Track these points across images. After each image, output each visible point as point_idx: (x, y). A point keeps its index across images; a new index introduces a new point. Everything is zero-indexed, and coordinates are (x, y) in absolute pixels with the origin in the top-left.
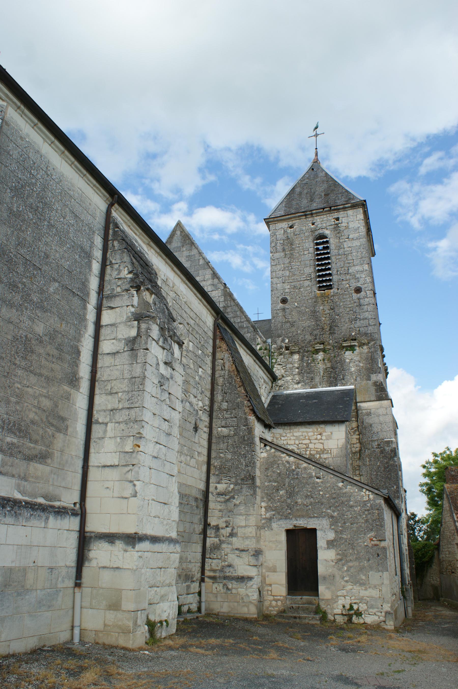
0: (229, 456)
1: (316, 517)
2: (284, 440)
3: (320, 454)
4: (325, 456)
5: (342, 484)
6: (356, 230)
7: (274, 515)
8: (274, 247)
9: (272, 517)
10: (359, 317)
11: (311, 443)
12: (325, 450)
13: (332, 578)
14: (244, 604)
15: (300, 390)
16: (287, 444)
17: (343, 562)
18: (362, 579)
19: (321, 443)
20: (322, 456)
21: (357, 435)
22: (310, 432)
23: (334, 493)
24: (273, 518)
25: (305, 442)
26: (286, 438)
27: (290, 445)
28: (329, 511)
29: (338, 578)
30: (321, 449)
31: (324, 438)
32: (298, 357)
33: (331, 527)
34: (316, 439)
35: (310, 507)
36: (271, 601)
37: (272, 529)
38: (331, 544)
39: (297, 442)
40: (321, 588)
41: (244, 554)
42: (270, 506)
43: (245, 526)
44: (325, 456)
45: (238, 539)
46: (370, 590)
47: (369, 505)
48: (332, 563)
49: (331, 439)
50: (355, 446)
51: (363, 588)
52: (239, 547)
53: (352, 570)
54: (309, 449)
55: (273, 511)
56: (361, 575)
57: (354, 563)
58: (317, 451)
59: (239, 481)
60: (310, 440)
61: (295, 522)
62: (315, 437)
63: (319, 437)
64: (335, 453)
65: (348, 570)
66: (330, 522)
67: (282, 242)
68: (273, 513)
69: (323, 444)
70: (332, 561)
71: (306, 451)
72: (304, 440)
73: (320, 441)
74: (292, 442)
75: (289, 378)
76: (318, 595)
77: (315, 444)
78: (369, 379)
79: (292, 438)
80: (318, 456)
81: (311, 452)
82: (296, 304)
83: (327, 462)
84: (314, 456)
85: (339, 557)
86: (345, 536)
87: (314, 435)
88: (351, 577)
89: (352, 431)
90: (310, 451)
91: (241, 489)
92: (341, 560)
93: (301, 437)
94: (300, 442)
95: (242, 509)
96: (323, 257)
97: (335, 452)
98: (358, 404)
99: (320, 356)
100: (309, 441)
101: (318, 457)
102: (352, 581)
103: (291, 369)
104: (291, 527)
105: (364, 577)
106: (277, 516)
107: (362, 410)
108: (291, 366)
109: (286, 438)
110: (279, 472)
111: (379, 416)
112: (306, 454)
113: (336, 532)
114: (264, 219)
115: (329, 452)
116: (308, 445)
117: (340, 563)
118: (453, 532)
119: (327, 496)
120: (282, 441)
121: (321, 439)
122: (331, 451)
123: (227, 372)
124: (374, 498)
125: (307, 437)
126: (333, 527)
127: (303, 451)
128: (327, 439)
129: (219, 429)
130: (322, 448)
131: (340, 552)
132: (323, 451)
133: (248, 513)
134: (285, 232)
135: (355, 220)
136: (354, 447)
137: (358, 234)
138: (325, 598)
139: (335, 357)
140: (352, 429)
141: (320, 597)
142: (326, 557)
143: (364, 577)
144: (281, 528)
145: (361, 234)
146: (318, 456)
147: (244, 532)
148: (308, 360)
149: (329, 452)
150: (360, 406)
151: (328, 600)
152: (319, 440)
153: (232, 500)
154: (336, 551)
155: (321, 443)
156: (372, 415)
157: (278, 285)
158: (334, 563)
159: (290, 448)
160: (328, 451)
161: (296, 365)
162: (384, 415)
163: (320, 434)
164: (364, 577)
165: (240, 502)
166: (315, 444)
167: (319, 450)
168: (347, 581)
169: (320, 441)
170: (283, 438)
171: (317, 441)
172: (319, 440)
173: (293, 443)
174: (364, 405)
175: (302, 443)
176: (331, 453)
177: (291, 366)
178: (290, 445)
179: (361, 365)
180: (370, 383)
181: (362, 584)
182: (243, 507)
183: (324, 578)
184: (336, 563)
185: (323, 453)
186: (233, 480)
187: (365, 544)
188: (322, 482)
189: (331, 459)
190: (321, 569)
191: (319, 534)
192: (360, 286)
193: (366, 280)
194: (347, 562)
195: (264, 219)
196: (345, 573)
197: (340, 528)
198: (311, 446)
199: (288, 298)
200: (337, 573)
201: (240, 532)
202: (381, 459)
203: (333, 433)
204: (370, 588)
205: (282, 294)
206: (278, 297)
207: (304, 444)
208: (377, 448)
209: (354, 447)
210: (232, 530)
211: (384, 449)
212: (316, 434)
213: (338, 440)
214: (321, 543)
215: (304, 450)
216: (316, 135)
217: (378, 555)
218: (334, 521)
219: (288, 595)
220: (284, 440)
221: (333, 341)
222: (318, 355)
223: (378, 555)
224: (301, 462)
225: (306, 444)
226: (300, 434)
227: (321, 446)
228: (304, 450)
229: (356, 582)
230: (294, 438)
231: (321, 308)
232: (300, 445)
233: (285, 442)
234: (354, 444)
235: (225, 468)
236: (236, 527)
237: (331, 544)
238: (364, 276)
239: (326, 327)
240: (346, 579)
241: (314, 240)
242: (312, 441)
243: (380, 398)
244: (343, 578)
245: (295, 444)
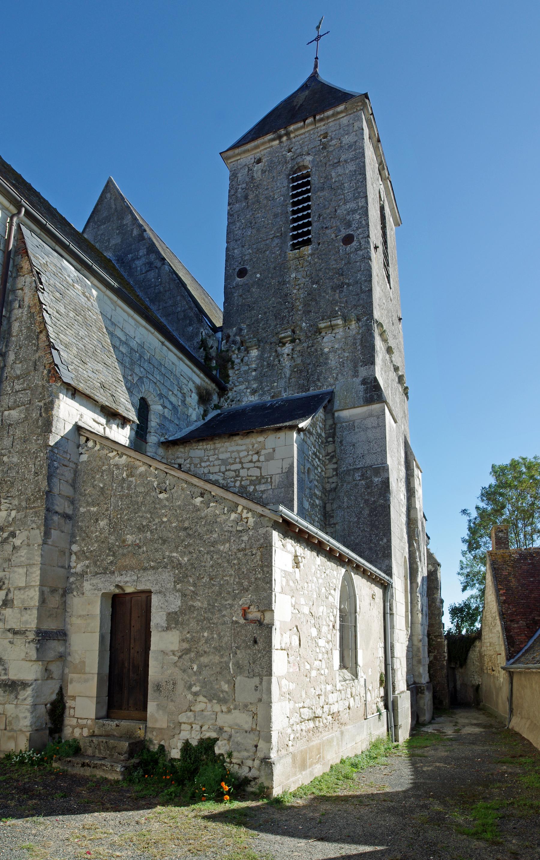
0: (15, 460)
1: (153, 568)
2: (204, 467)
3: (255, 485)
4: (262, 487)
5: (201, 499)
6: (350, 147)
7: (87, 567)
8: (233, 195)
9: (85, 570)
10: (347, 281)
11: (243, 468)
12: (263, 477)
13: (171, 687)
14: (10, 734)
15: (254, 399)
16: (209, 473)
17: (193, 655)
18: (222, 691)
19: (257, 467)
20: (257, 487)
21: (334, 463)
22: (243, 451)
23: (187, 519)
24: (87, 573)
25: (233, 467)
26: (208, 463)
27: (212, 474)
28: (175, 554)
29: (180, 686)
30: (257, 477)
31: (262, 458)
32: (256, 354)
33: (175, 586)
34: (251, 461)
35: (145, 549)
36: (74, 728)
37: (83, 594)
38: (174, 620)
39: (223, 469)
40: (151, 707)
41: (19, 640)
42: (83, 551)
43: (25, 588)
44: (262, 487)
45: (13, 611)
46: (236, 713)
47: (245, 538)
48: (173, 657)
49: (273, 459)
50: (331, 480)
51: (224, 709)
52: (14, 626)
53: (206, 673)
54: (239, 478)
55: (87, 558)
56: (223, 683)
57: (211, 657)
58: (251, 481)
59: (24, 504)
60: (241, 463)
61: (118, 579)
62: (249, 458)
63: (255, 458)
64: (277, 481)
65: (199, 672)
66: (175, 576)
67: (244, 186)
68: (87, 562)
69: (260, 468)
70: (174, 654)
71: (235, 481)
72: (233, 464)
73: (257, 464)
74: (216, 469)
75: (242, 387)
76: (144, 719)
77: (248, 469)
78: (356, 374)
79: (216, 463)
80: (251, 489)
81: (243, 483)
82: (258, 275)
83: (264, 496)
84: (246, 488)
85: (185, 645)
86: (198, 604)
87: (248, 455)
88: (204, 684)
89: (328, 457)
90: (241, 481)
91: (25, 517)
92: (187, 651)
93: (231, 461)
94: (228, 468)
95: (23, 554)
96: (300, 198)
97: (277, 480)
98: (336, 414)
99: (287, 349)
100: (240, 466)
101: (251, 490)
102: (205, 693)
103: (246, 372)
104: (112, 589)
105: (226, 687)
106: (93, 569)
107: (341, 423)
108: (246, 368)
109: (208, 463)
110: (102, 486)
111: (366, 429)
112: (235, 486)
113: (184, 595)
114: (220, 154)
115: (269, 480)
116: (239, 472)
117: (187, 657)
118: (494, 615)
119: (174, 525)
120: (203, 468)
121: (258, 461)
122: (271, 478)
123: (26, 309)
124: (256, 523)
125: (238, 460)
126: (178, 586)
127: (231, 482)
128: (267, 460)
129: (6, 413)
130: (259, 475)
131: (188, 635)
132: (260, 480)
133: (31, 562)
134: (249, 170)
135: (351, 131)
136: (328, 482)
137: (354, 153)
138: (158, 726)
139: (308, 347)
140: (326, 456)
141: (150, 724)
142: (164, 643)
143: (227, 686)
144: (96, 592)
145: (358, 151)
146: (251, 489)
147: (22, 597)
148: (270, 357)
149: (269, 480)
150: (339, 417)
151: (161, 729)
152: (255, 462)
153: (11, 539)
154: (181, 632)
155: (257, 467)
156: (357, 430)
157: (236, 251)
158: (176, 658)
159: (213, 477)
160: (267, 478)
161: (254, 366)
162: (375, 427)
163: (257, 453)
164: (226, 687)
165: (21, 541)
166: (248, 469)
167: (255, 478)
168: (196, 694)
169: (257, 464)
170: (203, 464)
171: (252, 465)
172: (255, 462)
173: (218, 471)
174: (345, 414)
175: (229, 470)
176: (271, 481)
177: (246, 368)
178: (212, 474)
179: (346, 354)
180: (358, 380)
181: (222, 701)
182: (25, 551)
183: (158, 687)
184: (180, 657)
185: (260, 483)
186: (16, 502)
187: (234, 619)
188: (167, 499)
189: (270, 492)
190: (154, 672)
191: (155, 600)
192: (352, 233)
193: (361, 222)
194: (199, 655)
195: (220, 154)
196: (194, 678)
197: (192, 588)
198: (243, 473)
199: (248, 268)
200: (178, 675)
201: (17, 597)
202: (367, 497)
203: (276, 449)
204: (235, 709)
205: (240, 263)
206: (234, 269)
207: (232, 471)
208: (360, 480)
209: (328, 482)
210: (7, 595)
211: (371, 481)
212: (250, 453)
213: (283, 459)
214: (157, 618)
215: (232, 480)
216: (318, 38)
217: (255, 642)
218: (182, 574)
219: (108, 716)
220: (204, 467)
221: (306, 324)
222: (284, 348)
223: (255, 642)
224: (138, 463)
225: (235, 471)
226: (228, 455)
227: (256, 472)
228: (232, 480)
229: (214, 696)
230: (220, 462)
231: (293, 275)
232: (227, 473)
233: (206, 471)
234: (328, 478)
235: (6, 482)
236: (12, 589)
237: (174, 620)
238: (358, 217)
239: (298, 304)
240: (195, 689)
241: (290, 175)
242: (244, 465)
243: (369, 401)
244: (190, 687)
245: (220, 472)
